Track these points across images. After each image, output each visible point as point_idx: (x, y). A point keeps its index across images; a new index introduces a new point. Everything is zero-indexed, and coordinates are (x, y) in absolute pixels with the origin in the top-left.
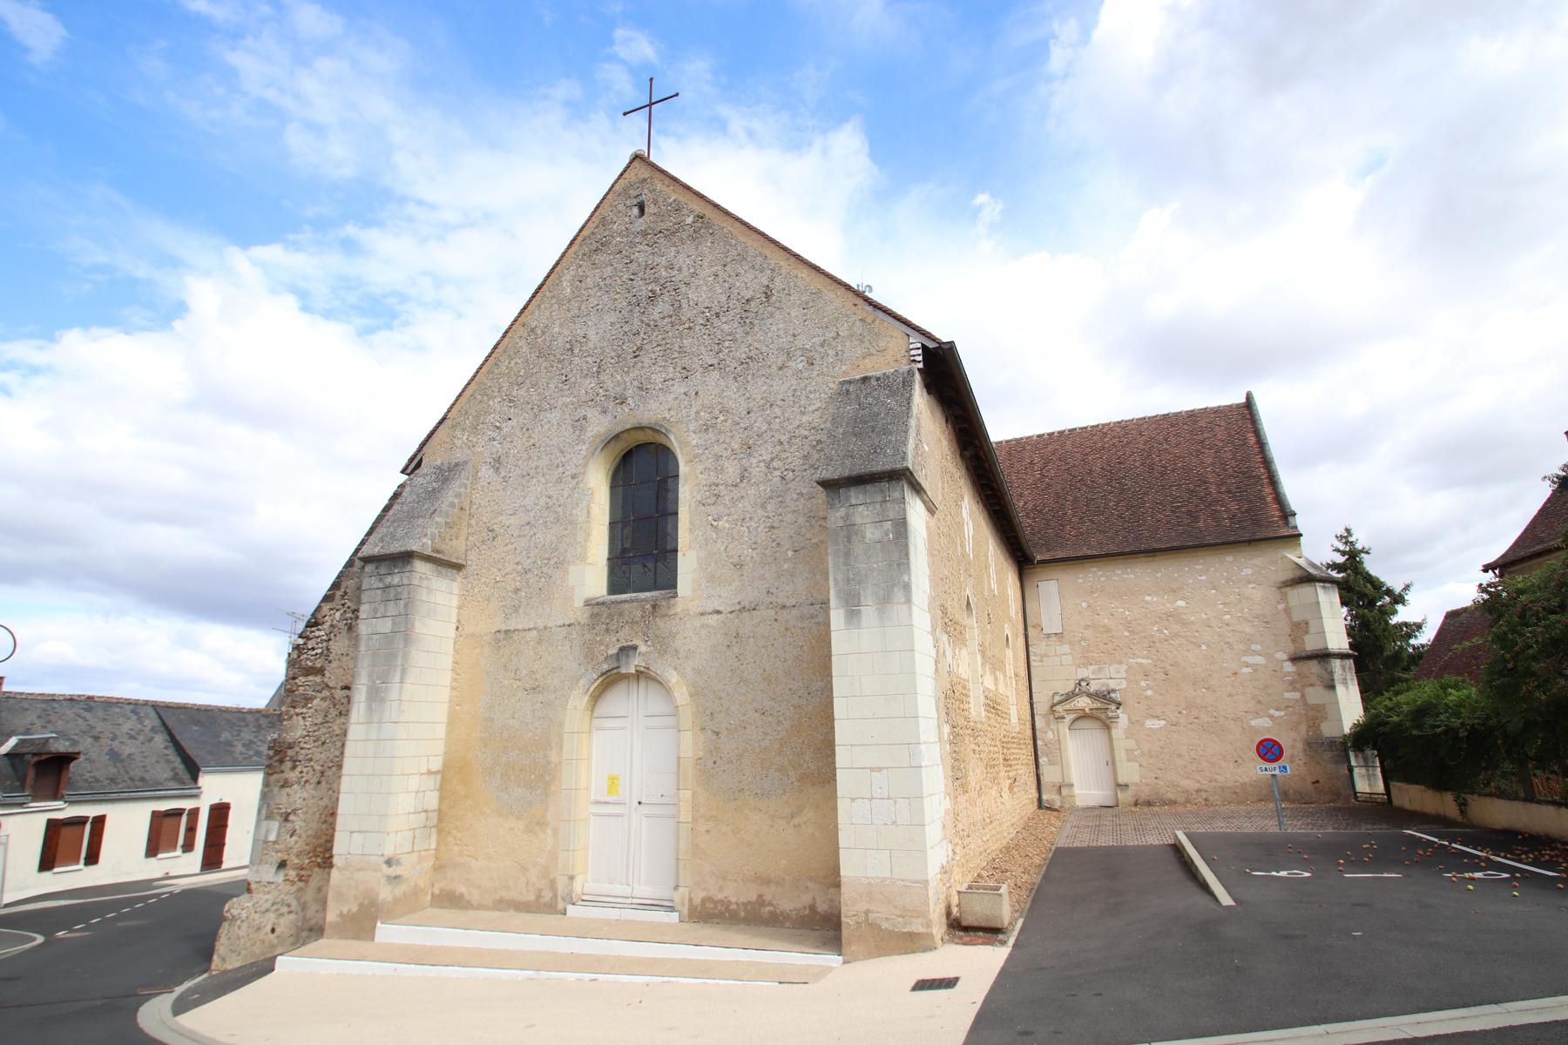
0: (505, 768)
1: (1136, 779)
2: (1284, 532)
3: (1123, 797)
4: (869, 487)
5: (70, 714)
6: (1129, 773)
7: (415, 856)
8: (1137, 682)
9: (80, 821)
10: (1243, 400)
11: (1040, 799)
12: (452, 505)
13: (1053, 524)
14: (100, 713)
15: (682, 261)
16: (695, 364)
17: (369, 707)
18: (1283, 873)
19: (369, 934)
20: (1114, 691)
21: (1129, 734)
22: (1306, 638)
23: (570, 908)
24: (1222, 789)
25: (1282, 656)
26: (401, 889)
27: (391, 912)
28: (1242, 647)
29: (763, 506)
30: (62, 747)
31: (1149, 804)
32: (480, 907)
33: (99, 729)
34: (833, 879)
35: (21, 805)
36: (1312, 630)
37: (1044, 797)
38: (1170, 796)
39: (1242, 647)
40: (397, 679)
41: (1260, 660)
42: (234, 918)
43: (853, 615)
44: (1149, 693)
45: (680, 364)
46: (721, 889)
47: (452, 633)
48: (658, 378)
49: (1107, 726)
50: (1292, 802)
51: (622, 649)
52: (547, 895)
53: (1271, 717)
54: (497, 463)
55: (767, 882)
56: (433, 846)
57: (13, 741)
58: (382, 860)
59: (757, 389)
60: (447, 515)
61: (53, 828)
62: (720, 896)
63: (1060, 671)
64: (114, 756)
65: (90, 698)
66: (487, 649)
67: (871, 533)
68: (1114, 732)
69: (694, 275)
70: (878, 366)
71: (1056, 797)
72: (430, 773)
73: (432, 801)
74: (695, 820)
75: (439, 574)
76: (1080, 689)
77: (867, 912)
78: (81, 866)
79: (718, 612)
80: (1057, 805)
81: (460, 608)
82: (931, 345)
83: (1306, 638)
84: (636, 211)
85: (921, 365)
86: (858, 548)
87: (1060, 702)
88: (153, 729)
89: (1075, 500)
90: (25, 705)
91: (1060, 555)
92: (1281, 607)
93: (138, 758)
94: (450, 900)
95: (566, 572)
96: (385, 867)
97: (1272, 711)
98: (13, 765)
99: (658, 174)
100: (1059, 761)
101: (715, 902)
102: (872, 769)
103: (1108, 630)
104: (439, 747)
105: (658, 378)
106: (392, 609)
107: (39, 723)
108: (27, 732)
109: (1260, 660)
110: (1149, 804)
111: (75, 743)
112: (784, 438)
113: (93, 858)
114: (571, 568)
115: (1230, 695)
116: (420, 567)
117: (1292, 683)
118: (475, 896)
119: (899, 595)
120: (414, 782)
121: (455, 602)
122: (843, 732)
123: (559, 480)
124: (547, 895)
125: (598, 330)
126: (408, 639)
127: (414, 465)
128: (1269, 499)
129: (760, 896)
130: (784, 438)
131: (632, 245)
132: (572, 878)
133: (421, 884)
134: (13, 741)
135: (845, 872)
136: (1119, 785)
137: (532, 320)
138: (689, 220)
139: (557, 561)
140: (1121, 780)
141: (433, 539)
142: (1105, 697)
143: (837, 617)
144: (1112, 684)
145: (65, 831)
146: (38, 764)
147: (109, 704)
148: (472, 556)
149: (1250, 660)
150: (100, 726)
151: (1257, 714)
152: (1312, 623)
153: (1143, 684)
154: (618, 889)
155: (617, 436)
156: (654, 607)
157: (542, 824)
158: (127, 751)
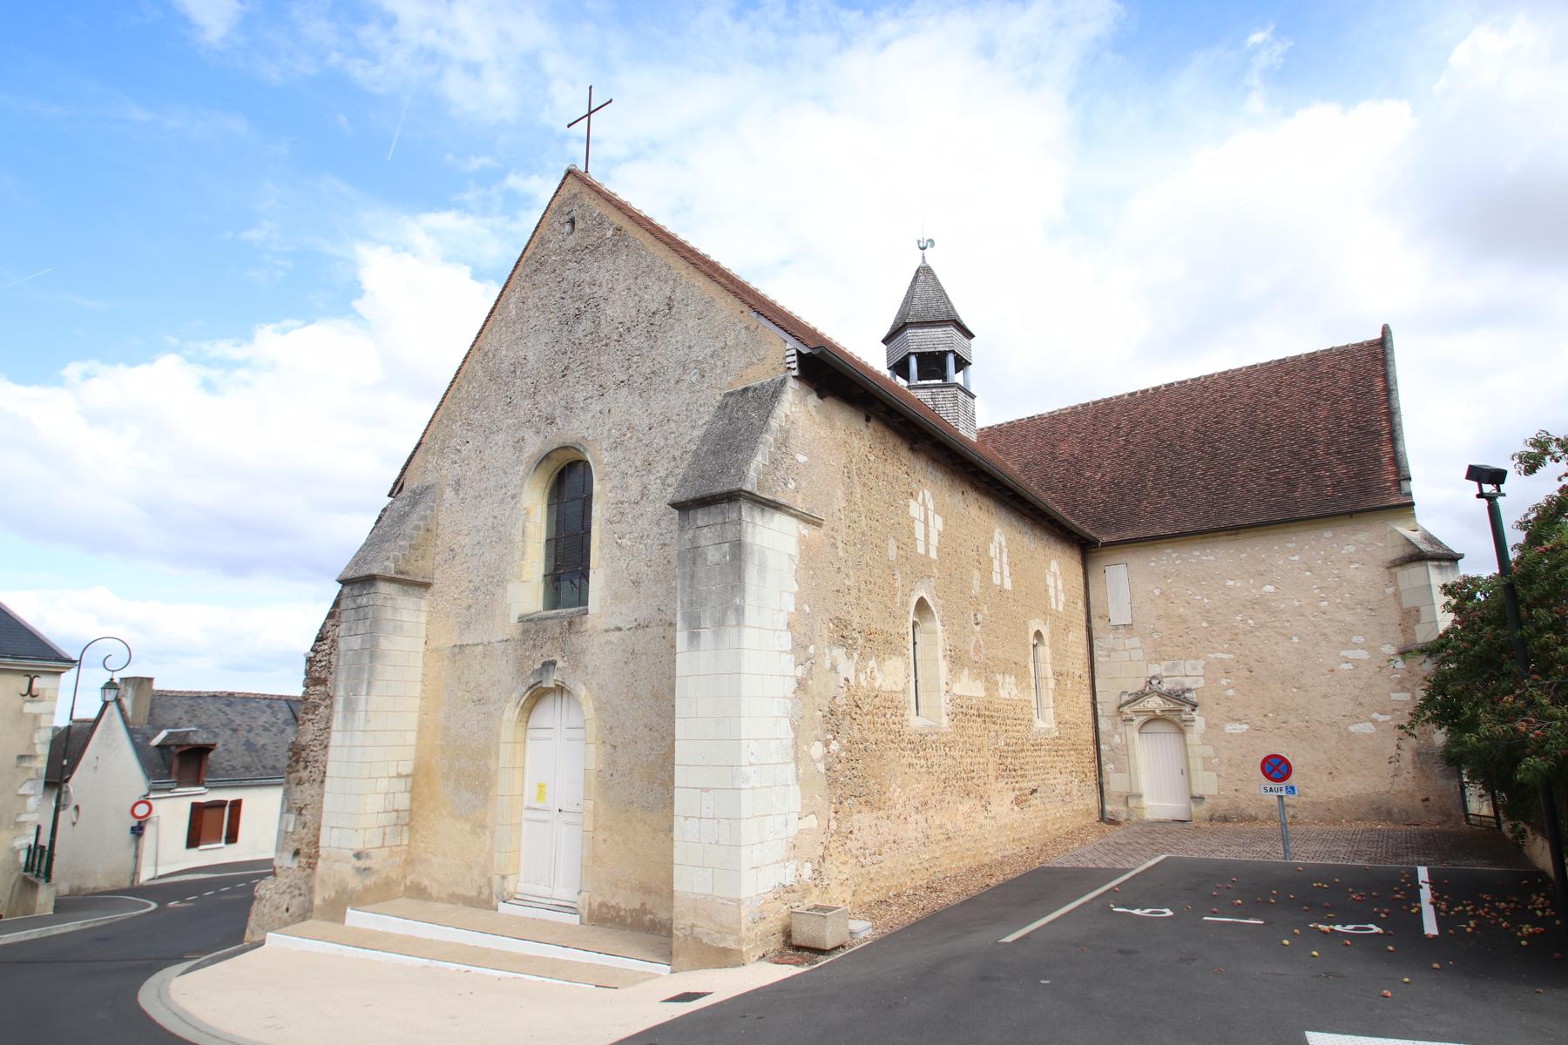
0: (453, 775)
2: (1394, 501)
3: (1201, 811)
4: (713, 508)
5: (213, 708)
6: (1206, 784)
7: (386, 851)
8: (1216, 680)
9: (220, 805)
10: (1379, 336)
11: (1102, 811)
12: (417, 528)
13: (1128, 499)
14: (239, 708)
15: (603, 277)
16: (609, 381)
17: (345, 717)
18: (1137, 912)
19: (339, 917)
20: (1189, 690)
21: (1205, 740)
22: (1417, 628)
23: (502, 906)
24: (1314, 804)
25: (1389, 650)
26: (371, 880)
27: (359, 900)
28: (1341, 638)
29: (658, 524)
30: (200, 739)
31: (1225, 819)
32: (439, 900)
33: (238, 722)
34: (666, 891)
35: (168, 790)
36: (1424, 618)
37: (1108, 808)
38: (1252, 811)
39: (1341, 638)
40: (364, 692)
41: (1363, 654)
42: (262, 898)
43: (694, 637)
44: (1231, 692)
45: (598, 381)
46: (613, 896)
47: (422, 648)
48: (580, 397)
49: (1181, 729)
50: (1396, 822)
51: (544, 664)
52: (486, 891)
53: (1374, 722)
54: (457, 486)
55: (648, 891)
56: (405, 842)
57: (164, 734)
58: (351, 853)
59: (657, 405)
60: (411, 538)
61: (197, 810)
62: (613, 902)
63: (1126, 667)
64: (250, 746)
65: (231, 694)
66: (446, 662)
67: (713, 555)
68: (1189, 737)
69: (612, 290)
70: (758, 376)
71: (1122, 808)
72: (399, 776)
73: (403, 801)
74: (595, 829)
75: (406, 593)
76: (1151, 687)
77: (693, 926)
78: (222, 844)
79: (619, 629)
80: (1122, 817)
81: (428, 623)
82: (805, 351)
83: (1417, 628)
84: (568, 227)
85: (795, 373)
86: (701, 572)
87: (1128, 703)
88: (286, 722)
89: (1159, 469)
90: (175, 702)
91: (1130, 535)
92: (1390, 590)
93: (271, 748)
94: (418, 892)
95: (505, 589)
96: (354, 860)
97: (1375, 715)
98: (163, 756)
99: (586, 189)
100: (1126, 766)
101: (609, 908)
102: (702, 789)
103: (1183, 620)
104: (410, 753)
105: (580, 397)
106: (361, 628)
107: (186, 718)
108: (176, 726)
109: (1363, 654)
110: (1225, 819)
111: (216, 735)
112: (677, 454)
113: (232, 837)
114: (510, 586)
115: (1325, 696)
116: (383, 588)
117: (1400, 682)
118: (434, 890)
119: (731, 618)
120: (383, 784)
121: (423, 618)
122: (683, 752)
123: (502, 501)
124: (486, 891)
125: (535, 351)
126: (373, 656)
127: (397, 488)
128: (1385, 460)
129: (643, 904)
130: (677, 454)
131: (564, 262)
132: (504, 877)
133: (393, 875)
134: (164, 734)
135: (676, 888)
136: (1193, 797)
137: (485, 344)
138: (610, 233)
139: (496, 579)
140: (1197, 791)
141: (396, 561)
142: (1178, 697)
143: (681, 638)
144: (1188, 683)
145: (208, 814)
146: (182, 755)
147: (247, 699)
148: (438, 574)
149: (1350, 654)
150: (238, 720)
151: (1356, 719)
152: (1423, 610)
153: (1224, 682)
154: (543, 890)
155: (547, 456)
156: (570, 624)
157: (483, 827)
158: (261, 742)
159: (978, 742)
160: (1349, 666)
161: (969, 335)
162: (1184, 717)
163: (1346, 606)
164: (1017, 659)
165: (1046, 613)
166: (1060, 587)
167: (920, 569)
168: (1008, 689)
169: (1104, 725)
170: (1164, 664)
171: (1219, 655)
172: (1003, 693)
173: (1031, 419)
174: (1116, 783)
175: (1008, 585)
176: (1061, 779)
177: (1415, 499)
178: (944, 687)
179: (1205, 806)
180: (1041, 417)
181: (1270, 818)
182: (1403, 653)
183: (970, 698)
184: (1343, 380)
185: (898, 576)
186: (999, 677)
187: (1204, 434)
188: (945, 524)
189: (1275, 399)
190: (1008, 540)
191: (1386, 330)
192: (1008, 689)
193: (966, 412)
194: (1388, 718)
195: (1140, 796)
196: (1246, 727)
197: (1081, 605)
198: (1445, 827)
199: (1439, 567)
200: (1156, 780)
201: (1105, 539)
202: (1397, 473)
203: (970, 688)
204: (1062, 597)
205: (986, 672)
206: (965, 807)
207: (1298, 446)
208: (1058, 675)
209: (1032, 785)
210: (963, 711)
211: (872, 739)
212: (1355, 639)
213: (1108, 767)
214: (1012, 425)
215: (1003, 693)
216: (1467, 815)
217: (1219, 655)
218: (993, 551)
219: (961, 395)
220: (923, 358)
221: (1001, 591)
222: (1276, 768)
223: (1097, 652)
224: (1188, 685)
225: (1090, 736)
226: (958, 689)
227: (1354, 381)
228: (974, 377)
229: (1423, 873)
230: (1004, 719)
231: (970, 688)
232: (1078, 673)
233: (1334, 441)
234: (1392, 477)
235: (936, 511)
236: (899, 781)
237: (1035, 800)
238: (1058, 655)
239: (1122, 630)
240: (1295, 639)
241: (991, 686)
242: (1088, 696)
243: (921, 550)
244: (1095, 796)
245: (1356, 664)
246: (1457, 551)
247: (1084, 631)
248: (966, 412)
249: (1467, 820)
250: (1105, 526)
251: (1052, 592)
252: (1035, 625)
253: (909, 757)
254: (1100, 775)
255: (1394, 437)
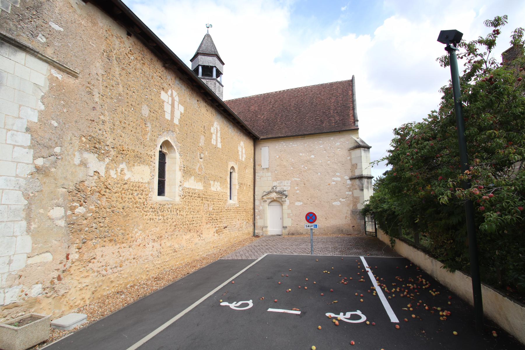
1: (290, 225)
3: (286, 231)
6: (288, 223)
11: (254, 232)
13: (271, 125)
20: (285, 191)
21: (289, 207)
25: (347, 177)
31: (293, 234)
36: (358, 167)
37: (256, 231)
38: (301, 231)
41: (339, 179)
44: (298, 191)
53: (340, 201)
63: (265, 183)
87: (265, 195)
91: (270, 136)
92: (349, 158)
97: (341, 199)
109: (339, 179)
110: (293, 234)
117: (349, 188)
140: (285, 225)
151: (335, 200)
153: (296, 188)
159: (197, 208)
160: (335, 183)
161: (223, 64)
162: (283, 200)
163: (335, 163)
164: (222, 176)
165: (237, 160)
166: (244, 152)
167: (169, 127)
168: (216, 187)
169: (257, 203)
170: (278, 182)
171: (296, 179)
172: (213, 189)
173: (243, 98)
174: (259, 223)
175: (219, 145)
176: (239, 222)
177: (359, 127)
178: (178, 183)
179: (287, 230)
180: (246, 98)
181: (307, 233)
182: (351, 179)
183: (195, 190)
184: (340, 91)
185: (149, 124)
186: (212, 182)
187: (297, 105)
188: (185, 110)
189: (319, 96)
190: (221, 128)
191: (353, 77)
192: (216, 187)
193: (219, 91)
194: (344, 200)
195: (267, 227)
196: (302, 203)
197: (252, 160)
198: (359, 236)
199: (364, 150)
200: (273, 221)
201: (262, 137)
202: (354, 119)
203: (194, 184)
204: (244, 156)
205: (205, 179)
206: (188, 236)
207: (325, 112)
208: (241, 184)
209: (225, 225)
210: (188, 195)
211: (120, 206)
212: (337, 174)
213: (257, 217)
214: (236, 100)
215: (213, 189)
216: (366, 232)
217: (296, 179)
218: (213, 130)
219: (217, 84)
220: (204, 67)
221: (216, 147)
222: (311, 218)
223: (257, 177)
224: (285, 189)
225: (252, 207)
226: (187, 185)
227: (343, 91)
228: (223, 79)
229: (362, 258)
230: (213, 199)
231: (194, 184)
232: (249, 184)
233: (336, 109)
234: (352, 121)
235: (180, 103)
236: (141, 227)
237: (226, 231)
238: (240, 176)
239: (265, 170)
240: (319, 174)
241: (207, 185)
242: (252, 193)
243: (168, 117)
244: (252, 227)
245: (337, 182)
246: (370, 145)
247: (252, 170)
248: (219, 91)
249: (366, 233)
250: (262, 133)
251: (240, 153)
252: (231, 164)
253: (151, 215)
254: (254, 220)
255: (354, 109)
